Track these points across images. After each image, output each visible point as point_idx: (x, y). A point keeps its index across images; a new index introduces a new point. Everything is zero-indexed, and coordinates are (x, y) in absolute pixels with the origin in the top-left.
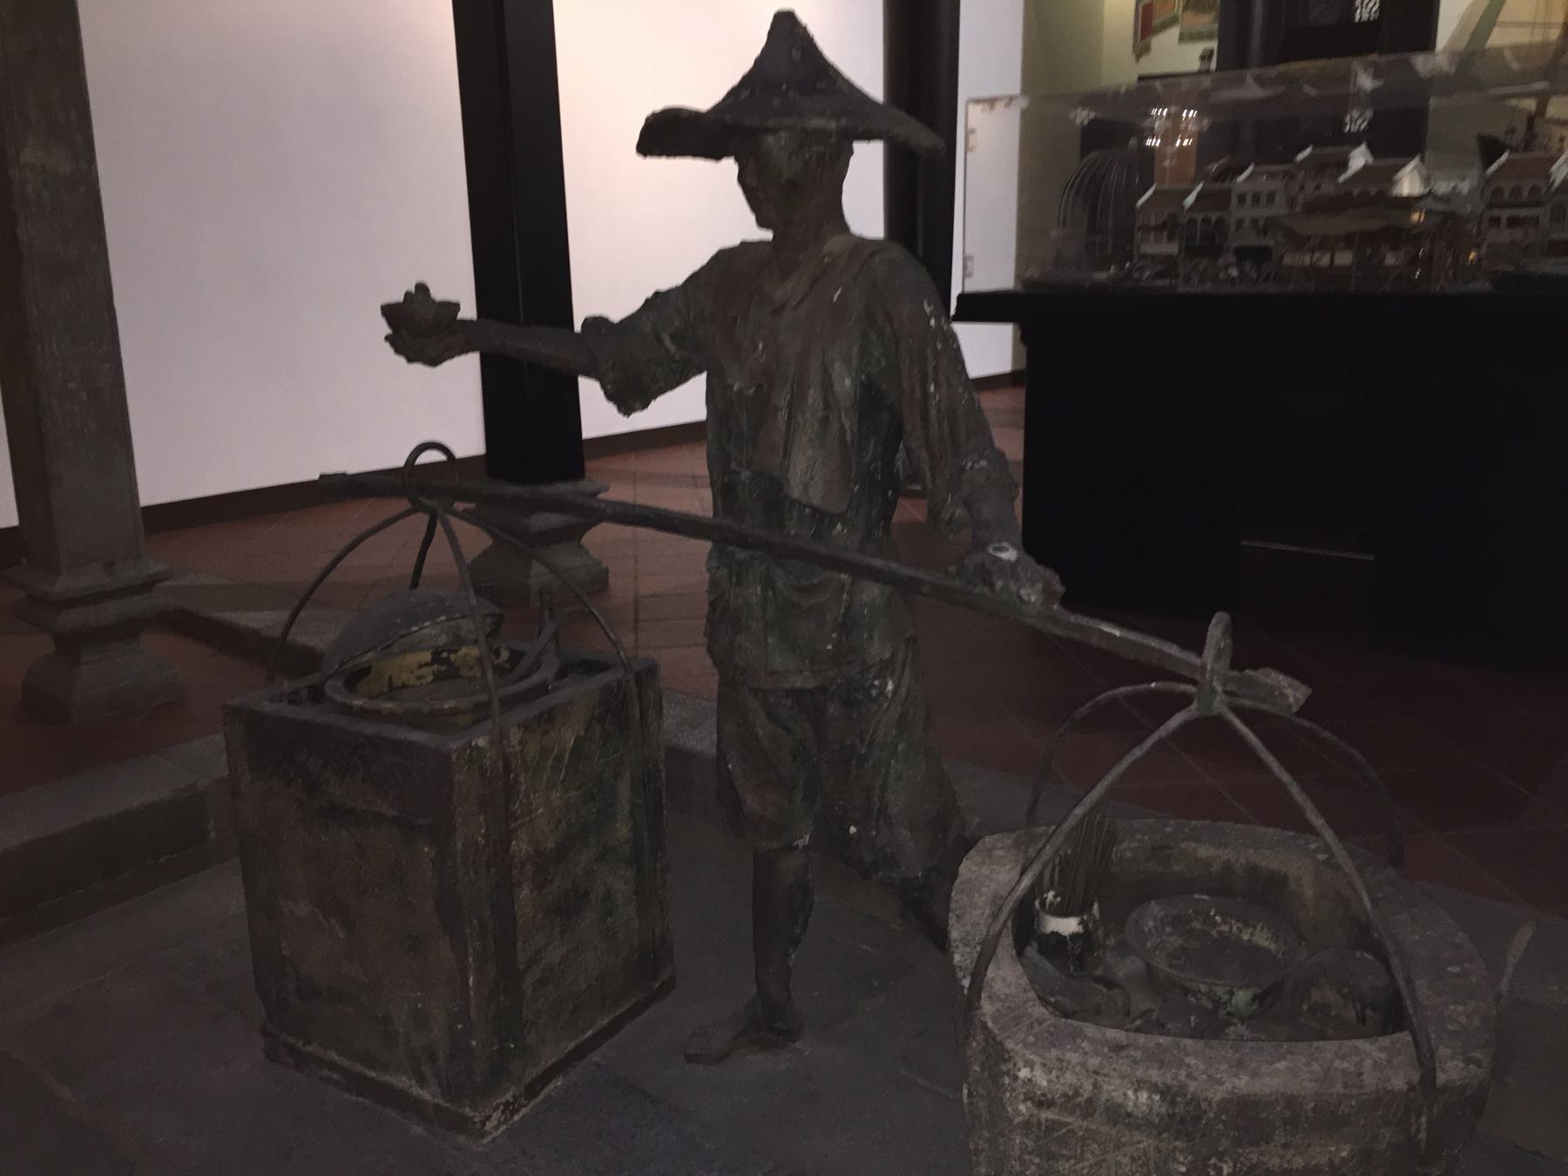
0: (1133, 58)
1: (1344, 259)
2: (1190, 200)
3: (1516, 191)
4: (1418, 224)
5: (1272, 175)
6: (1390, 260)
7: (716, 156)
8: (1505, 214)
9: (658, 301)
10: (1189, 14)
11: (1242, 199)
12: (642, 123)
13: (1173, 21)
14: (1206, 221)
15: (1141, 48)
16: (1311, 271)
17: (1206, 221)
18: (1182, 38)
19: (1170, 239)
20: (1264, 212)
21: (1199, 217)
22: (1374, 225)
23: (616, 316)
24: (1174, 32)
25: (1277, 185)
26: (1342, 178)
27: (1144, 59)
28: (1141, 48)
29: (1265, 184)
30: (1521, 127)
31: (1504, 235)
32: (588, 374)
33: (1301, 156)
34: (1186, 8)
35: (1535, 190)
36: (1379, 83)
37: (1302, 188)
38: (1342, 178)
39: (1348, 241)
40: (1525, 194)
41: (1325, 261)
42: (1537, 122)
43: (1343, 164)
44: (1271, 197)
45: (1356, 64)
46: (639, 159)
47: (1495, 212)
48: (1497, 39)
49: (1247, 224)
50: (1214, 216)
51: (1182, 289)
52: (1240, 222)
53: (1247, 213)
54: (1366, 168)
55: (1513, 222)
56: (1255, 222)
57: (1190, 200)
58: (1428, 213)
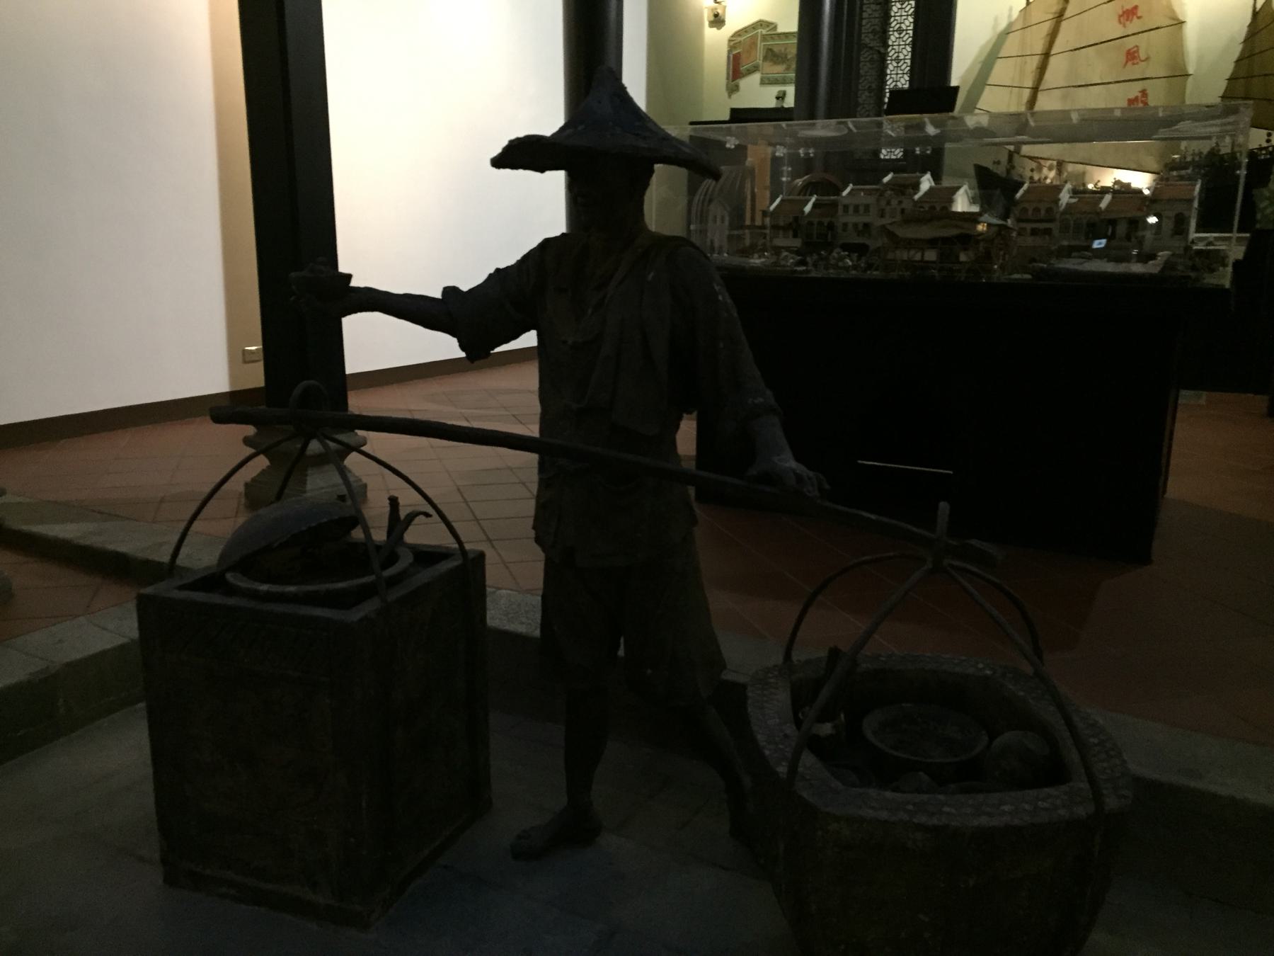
0: (726, 94)
1: (931, 255)
2: (808, 208)
3: (1037, 210)
4: (981, 234)
5: (869, 193)
6: (963, 258)
7: (652, 171)
8: (1029, 226)
9: (499, 276)
10: (767, 64)
11: (846, 207)
12: (505, 143)
13: (755, 69)
14: (820, 223)
15: (733, 89)
16: (909, 265)
17: (820, 223)
18: (763, 82)
19: (795, 236)
20: (861, 219)
21: (816, 220)
22: (955, 232)
23: (465, 288)
24: (756, 77)
25: (870, 200)
26: (916, 197)
27: (734, 96)
28: (733, 89)
29: (863, 199)
30: (1004, 159)
31: (1029, 241)
32: (539, 336)
33: (886, 179)
34: (765, 58)
35: (1049, 210)
36: (938, 131)
37: (888, 203)
38: (916, 197)
39: (932, 243)
40: (1043, 212)
41: (918, 257)
42: (1016, 156)
43: (916, 186)
44: (867, 207)
45: (926, 118)
46: (494, 170)
47: (1023, 225)
48: (1046, 103)
49: (850, 226)
50: (826, 221)
51: (813, 274)
52: (845, 225)
53: (852, 219)
54: (931, 189)
55: (1034, 232)
56: (855, 225)
57: (808, 208)
58: (989, 225)
